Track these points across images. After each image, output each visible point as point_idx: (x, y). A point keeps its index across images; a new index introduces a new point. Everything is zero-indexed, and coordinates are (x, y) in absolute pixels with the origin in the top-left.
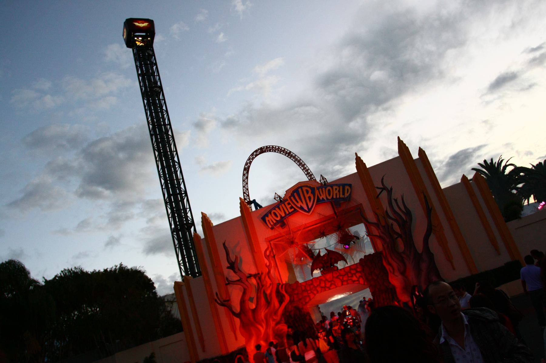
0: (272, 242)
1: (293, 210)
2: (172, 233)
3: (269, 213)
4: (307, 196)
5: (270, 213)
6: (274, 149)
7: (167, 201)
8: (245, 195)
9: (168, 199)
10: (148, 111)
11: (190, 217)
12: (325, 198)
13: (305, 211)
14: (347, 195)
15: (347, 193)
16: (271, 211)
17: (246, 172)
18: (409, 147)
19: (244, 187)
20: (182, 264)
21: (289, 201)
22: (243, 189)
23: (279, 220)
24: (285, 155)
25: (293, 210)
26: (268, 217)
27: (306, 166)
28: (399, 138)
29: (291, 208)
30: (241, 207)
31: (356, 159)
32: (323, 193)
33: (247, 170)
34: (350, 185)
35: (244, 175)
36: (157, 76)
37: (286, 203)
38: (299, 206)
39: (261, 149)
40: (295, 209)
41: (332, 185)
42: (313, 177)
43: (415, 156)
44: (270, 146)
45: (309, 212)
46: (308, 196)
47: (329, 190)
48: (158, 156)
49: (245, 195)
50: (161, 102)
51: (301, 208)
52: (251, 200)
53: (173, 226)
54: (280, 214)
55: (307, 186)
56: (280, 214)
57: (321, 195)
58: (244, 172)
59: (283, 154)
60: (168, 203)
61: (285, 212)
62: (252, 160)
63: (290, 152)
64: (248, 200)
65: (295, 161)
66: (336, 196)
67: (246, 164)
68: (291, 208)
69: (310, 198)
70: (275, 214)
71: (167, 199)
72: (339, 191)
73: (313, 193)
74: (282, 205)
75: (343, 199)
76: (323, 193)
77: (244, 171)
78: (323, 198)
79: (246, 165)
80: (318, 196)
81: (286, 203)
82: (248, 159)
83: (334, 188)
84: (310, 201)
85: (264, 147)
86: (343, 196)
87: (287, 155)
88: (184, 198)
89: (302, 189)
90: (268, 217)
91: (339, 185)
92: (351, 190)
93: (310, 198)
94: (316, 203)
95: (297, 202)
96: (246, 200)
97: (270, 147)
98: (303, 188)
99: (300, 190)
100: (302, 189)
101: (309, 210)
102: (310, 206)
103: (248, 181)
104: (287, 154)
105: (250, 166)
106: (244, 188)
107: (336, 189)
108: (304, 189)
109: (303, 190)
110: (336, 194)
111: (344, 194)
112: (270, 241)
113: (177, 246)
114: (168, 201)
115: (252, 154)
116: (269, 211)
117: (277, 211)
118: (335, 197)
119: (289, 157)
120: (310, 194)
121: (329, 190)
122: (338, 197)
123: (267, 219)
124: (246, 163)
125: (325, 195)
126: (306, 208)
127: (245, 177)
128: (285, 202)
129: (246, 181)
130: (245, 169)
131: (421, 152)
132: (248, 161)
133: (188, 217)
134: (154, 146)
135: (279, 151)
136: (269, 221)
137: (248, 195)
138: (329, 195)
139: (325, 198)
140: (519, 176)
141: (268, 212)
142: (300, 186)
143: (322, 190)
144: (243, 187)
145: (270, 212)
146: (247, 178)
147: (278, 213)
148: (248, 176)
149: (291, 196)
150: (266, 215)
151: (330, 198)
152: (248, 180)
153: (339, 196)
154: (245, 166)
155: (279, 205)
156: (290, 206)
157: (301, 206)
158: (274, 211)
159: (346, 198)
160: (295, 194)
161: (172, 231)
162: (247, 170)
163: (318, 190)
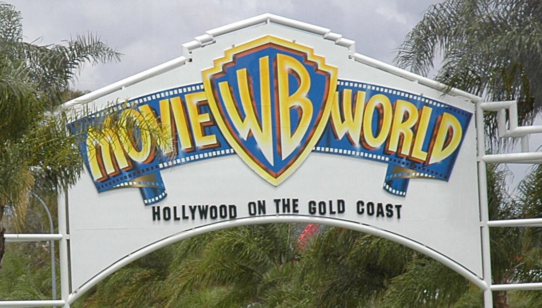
1: (212, 140)
4: (286, 103)
14: (438, 156)
21: (207, 96)
25: (212, 140)
38: (244, 136)
55: (301, 57)
66: (400, 147)
68: (209, 128)
69: (296, 115)
72: (415, 129)
73: (318, 96)
78: (347, 135)
81: (193, 101)
84: (293, 129)
95: (242, 117)
99: (264, 62)
102: (289, 146)
107: (406, 117)
108: (286, 64)
110: (402, 137)
111: (428, 148)
118: (393, 148)
120: (301, 99)
126: (265, 146)
136: (98, 150)
138: (376, 133)
156: (206, 118)
157: (251, 137)
160: (241, 74)
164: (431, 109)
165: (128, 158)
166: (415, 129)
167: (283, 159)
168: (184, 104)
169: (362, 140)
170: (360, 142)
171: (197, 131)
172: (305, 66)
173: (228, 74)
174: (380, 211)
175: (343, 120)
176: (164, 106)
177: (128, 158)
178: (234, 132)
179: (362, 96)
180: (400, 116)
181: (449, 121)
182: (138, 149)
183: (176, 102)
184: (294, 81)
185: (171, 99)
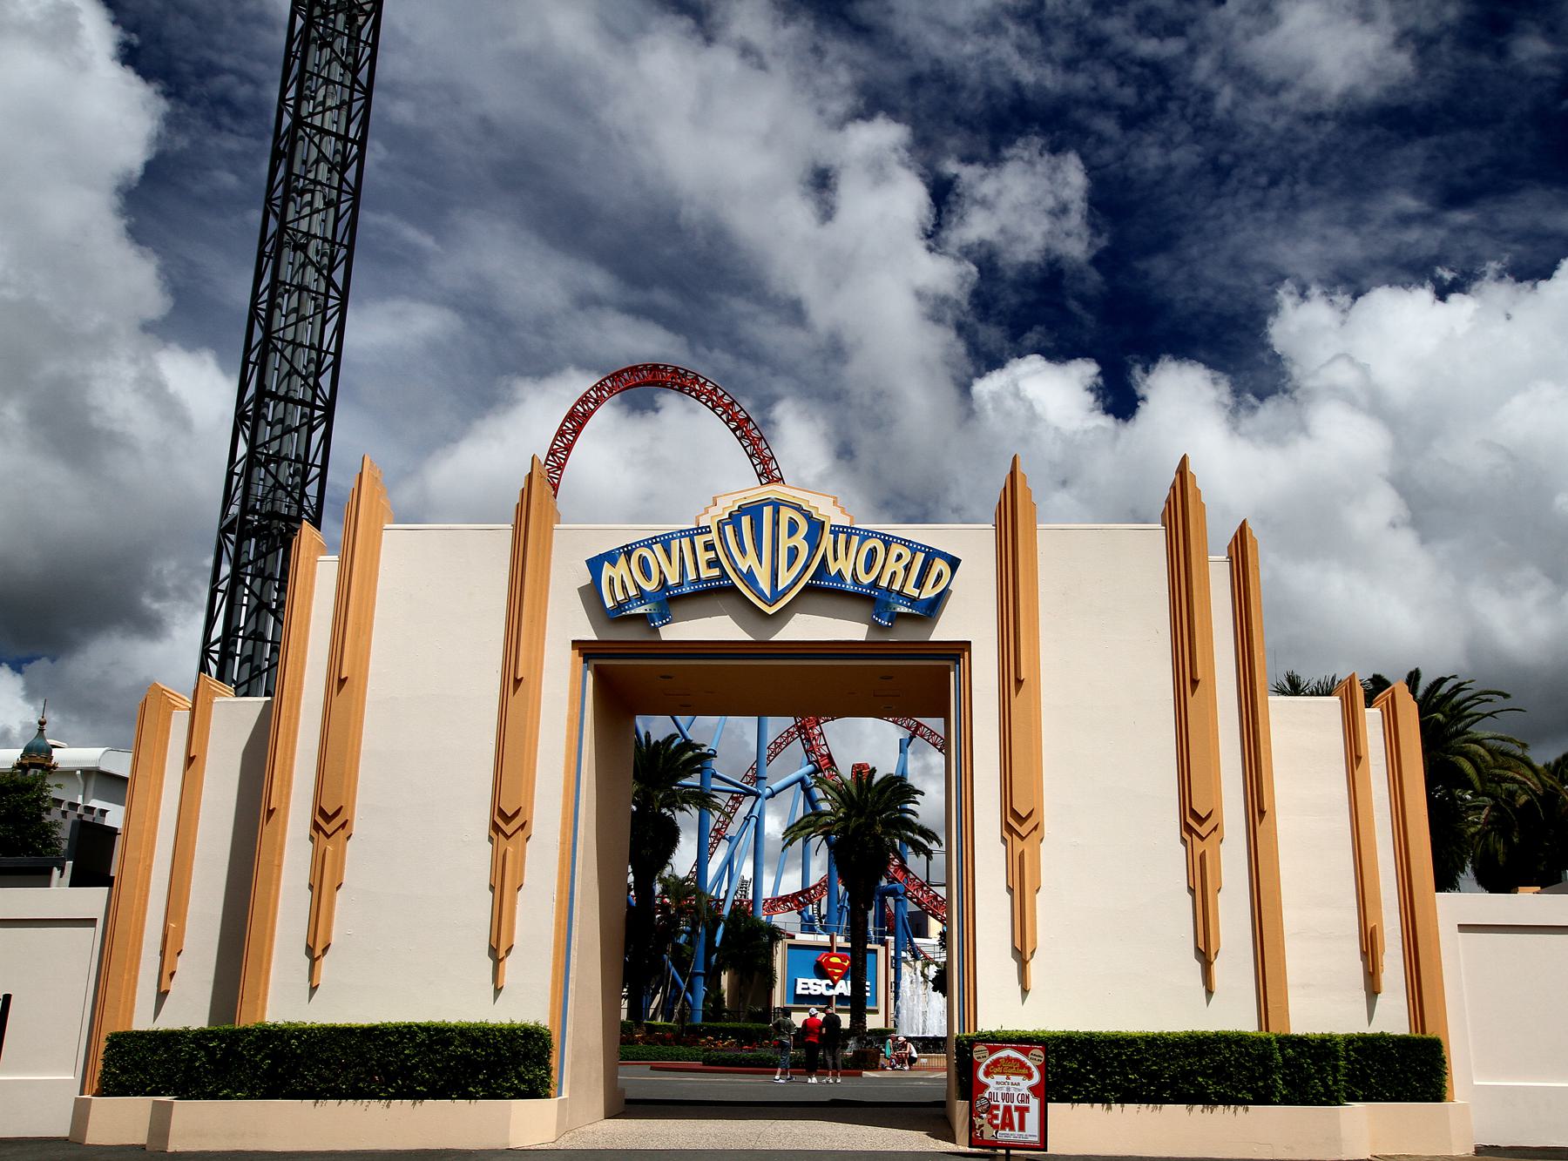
1: (716, 572)
2: (224, 531)
3: (625, 553)
4: (785, 543)
5: (628, 554)
6: (697, 387)
7: (244, 412)
9: (251, 407)
10: (297, 61)
11: (313, 501)
14: (928, 593)
16: (633, 550)
17: (570, 426)
20: (216, 657)
23: (650, 593)
24: (727, 423)
25: (716, 572)
26: (614, 563)
28: (1184, 459)
36: (366, 43)
37: (700, 541)
40: (724, 575)
41: (889, 536)
44: (687, 371)
47: (873, 551)
48: (273, 236)
50: (361, 49)
53: (234, 510)
55: (798, 508)
57: (836, 559)
58: (567, 424)
59: (720, 416)
60: (248, 418)
65: (753, 455)
66: (891, 581)
67: (580, 400)
69: (793, 553)
71: (248, 405)
72: (907, 568)
73: (813, 540)
74: (680, 542)
75: (913, 601)
77: (565, 420)
78: (839, 571)
79: (583, 402)
80: (824, 558)
81: (700, 541)
82: (596, 386)
83: (896, 549)
84: (790, 565)
85: (666, 366)
86: (915, 593)
88: (315, 423)
89: (776, 512)
90: (614, 563)
93: (793, 553)
94: (811, 579)
95: (743, 551)
97: (685, 375)
98: (782, 509)
99: (767, 512)
100: (776, 512)
103: (566, 460)
105: (593, 411)
107: (899, 557)
108: (786, 514)
111: (920, 584)
113: (223, 587)
114: (250, 413)
116: (627, 546)
118: (884, 583)
119: (738, 433)
121: (873, 551)
122: (896, 587)
123: (607, 571)
124: (585, 396)
127: (562, 442)
128: (698, 534)
130: (571, 416)
132: (592, 392)
133: (307, 496)
134: (274, 197)
135: (713, 401)
136: (611, 580)
138: (868, 570)
141: (622, 548)
146: (569, 448)
149: (728, 524)
151: (866, 579)
152: (567, 456)
153: (903, 586)
154: (577, 403)
155: (674, 538)
156: (712, 555)
158: (645, 552)
160: (746, 521)
161: (225, 523)
164: (924, 554)
165: (638, 587)
166: (907, 568)
168: (693, 543)
169: (854, 575)
170: (646, 737)
172: (801, 513)
173: (734, 519)
174: (1007, 1121)
175: (836, 559)
176: (675, 544)
177: (638, 587)
179: (856, 539)
181: (940, 565)
182: (867, 572)
183: (686, 542)
184: (793, 528)
185: (682, 540)
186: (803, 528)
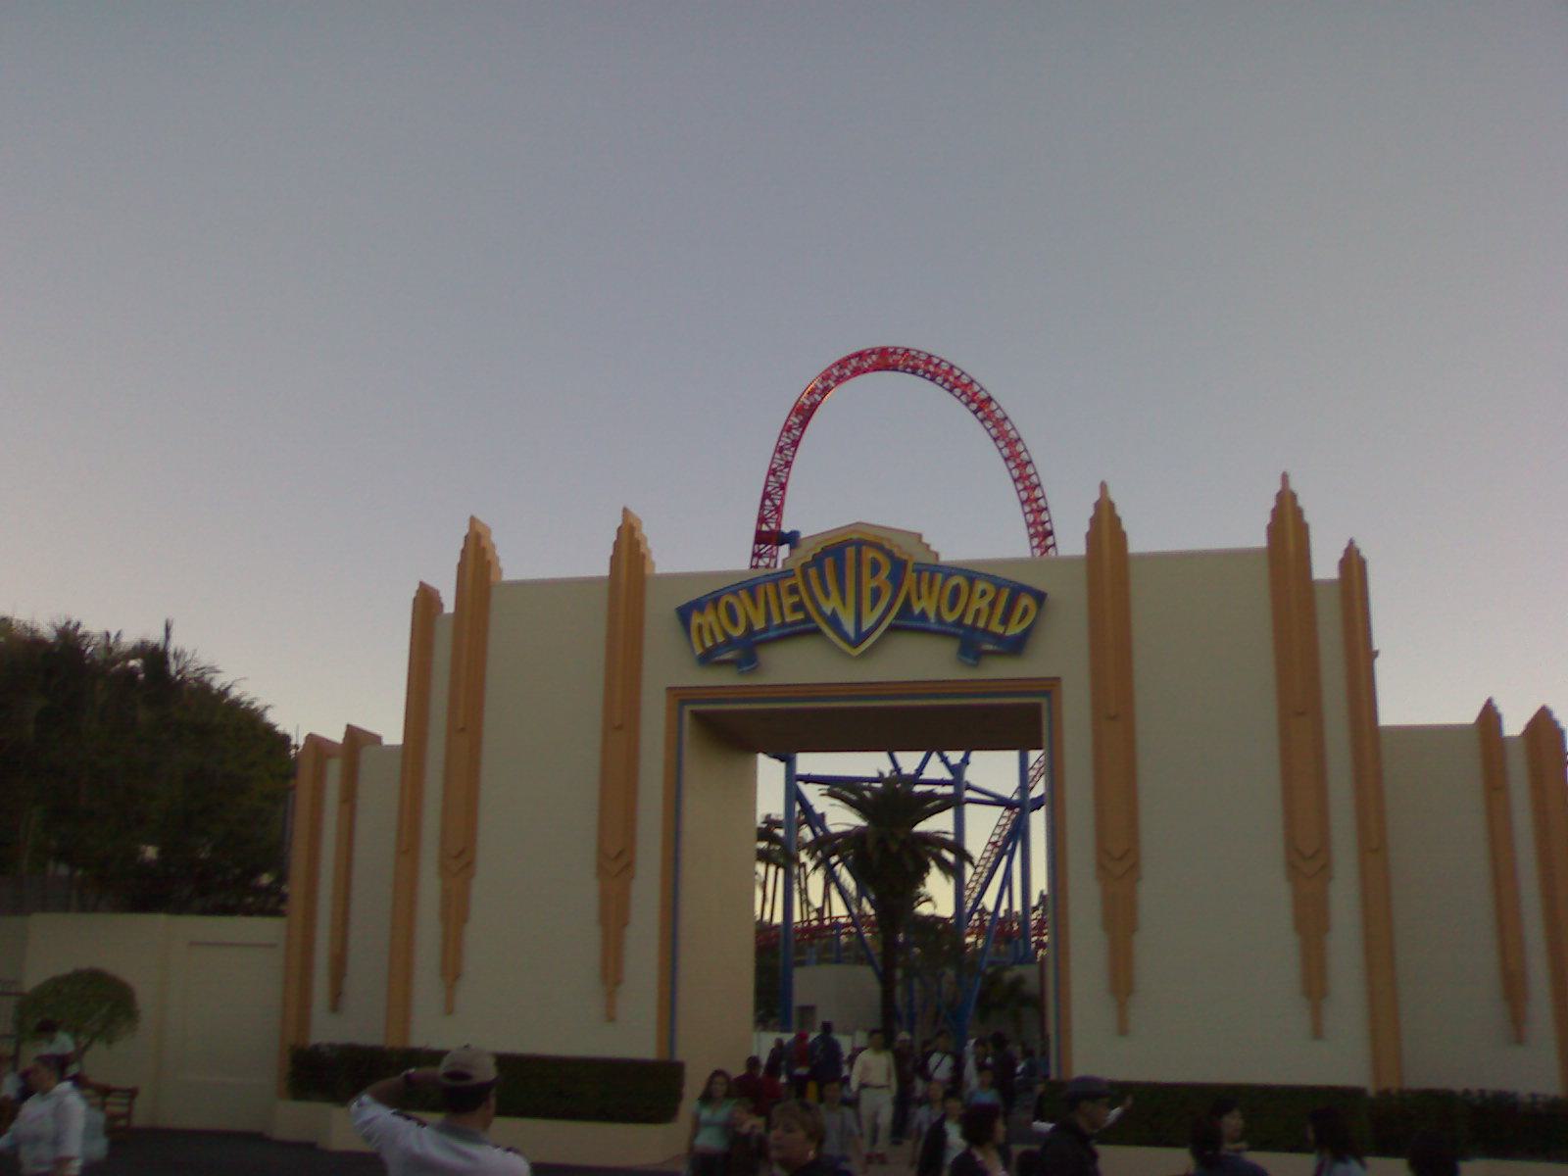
0: (688, 708)
1: (800, 616)
4: (869, 584)
8: (768, 502)
12: (932, 615)
13: (844, 636)
14: (1015, 629)
15: (1021, 620)
18: (864, 520)
19: (772, 472)
21: (798, 581)
22: (767, 481)
25: (800, 616)
27: (1014, 471)
29: (798, 607)
30: (617, 545)
31: (1098, 506)
32: (930, 593)
33: (804, 413)
34: (1040, 597)
35: (788, 429)
38: (829, 612)
39: (883, 352)
40: (808, 619)
42: (1028, 516)
43: (1325, 567)
45: (855, 644)
46: (874, 584)
49: (768, 502)
51: (834, 621)
52: (786, 528)
54: (748, 617)
55: (877, 546)
56: (748, 617)
61: (769, 618)
62: (835, 381)
63: (990, 399)
64: (773, 526)
68: (798, 607)
69: (876, 595)
70: (730, 608)
72: (992, 605)
75: (999, 638)
76: (930, 593)
78: (923, 615)
83: (980, 586)
85: (896, 348)
86: (1000, 630)
87: (974, 406)
89: (859, 553)
91: (999, 584)
92: (1037, 615)
93: (876, 595)
94: (896, 618)
95: (827, 595)
96: (767, 524)
98: (864, 548)
99: (850, 552)
100: (859, 553)
101: (862, 637)
104: (973, 401)
106: (772, 478)
107: (984, 593)
108: (870, 554)
109: (864, 555)
110: (978, 612)
112: (683, 702)
115: (842, 364)
117: (743, 605)
118: (968, 621)
119: (980, 414)
122: (981, 624)
123: (696, 619)
125: (762, 604)
126: (849, 626)
127: (788, 438)
129: (786, 455)
131: (1353, 564)
136: (700, 628)
137: (778, 510)
138: (952, 607)
139: (932, 615)
140: (818, 830)
142: (855, 536)
143: (822, 577)
144: (769, 474)
145: (715, 599)
147: (745, 609)
148: (800, 437)
150: (697, 605)
156: (796, 599)
157: (834, 613)
158: (731, 599)
159: (1008, 637)
160: (829, 562)
162: (804, 413)
163: (915, 575)
167: (863, 824)
171: (787, 611)
175: (919, 598)
178: (818, 607)
179: (939, 577)
180: (977, 594)
184: (876, 567)
186: (885, 573)
